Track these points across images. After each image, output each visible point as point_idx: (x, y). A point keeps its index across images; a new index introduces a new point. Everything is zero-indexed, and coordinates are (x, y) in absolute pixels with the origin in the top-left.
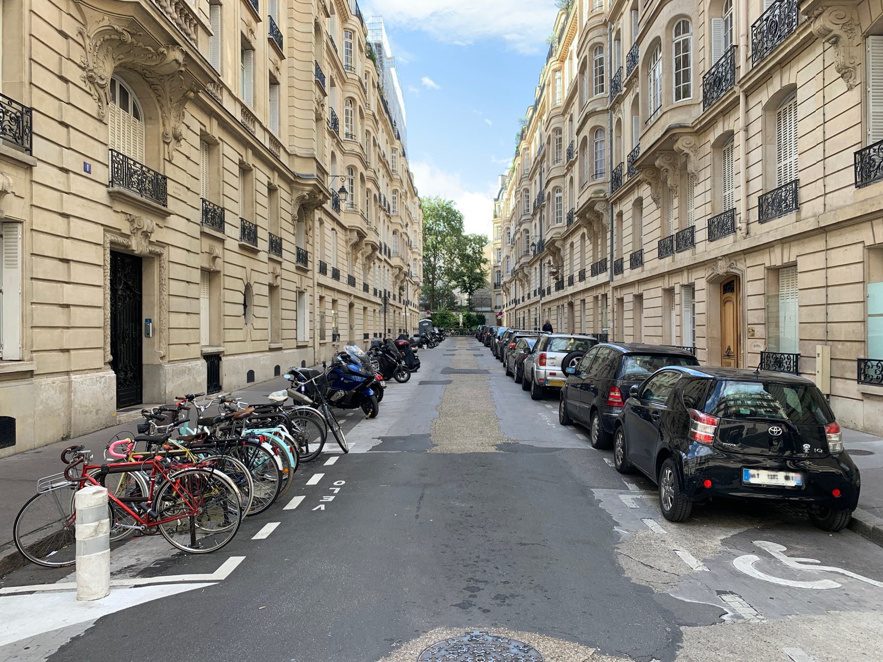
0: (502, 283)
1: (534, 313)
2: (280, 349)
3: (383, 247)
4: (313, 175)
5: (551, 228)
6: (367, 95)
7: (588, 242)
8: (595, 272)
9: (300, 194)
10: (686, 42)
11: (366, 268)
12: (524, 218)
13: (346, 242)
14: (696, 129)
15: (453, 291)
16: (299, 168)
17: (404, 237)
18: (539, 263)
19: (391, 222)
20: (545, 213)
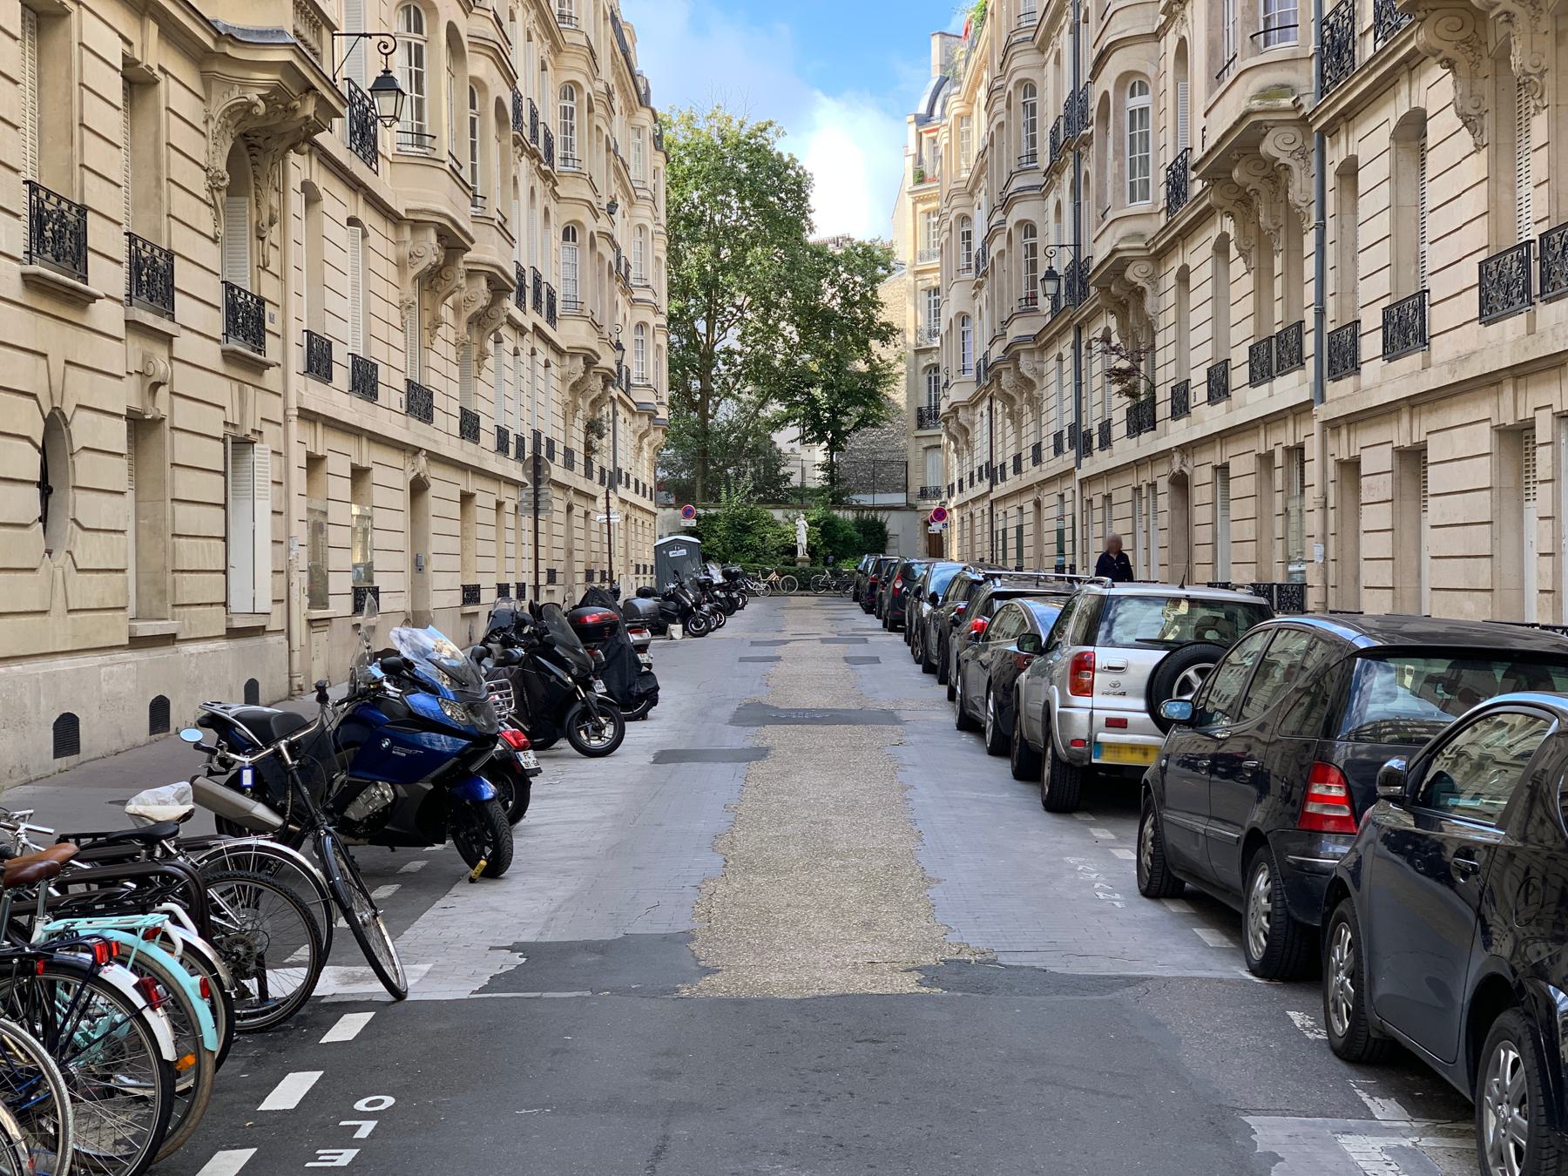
0: (944, 408)
1: (1054, 512)
2: (169, 639)
3: (529, 282)
4: (281, 32)
5: (1110, 216)
7: (1238, 267)
8: (1261, 372)
11: (471, 359)
15: (776, 436)
17: (603, 247)
18: (1070, 338)
19: (557, 198)
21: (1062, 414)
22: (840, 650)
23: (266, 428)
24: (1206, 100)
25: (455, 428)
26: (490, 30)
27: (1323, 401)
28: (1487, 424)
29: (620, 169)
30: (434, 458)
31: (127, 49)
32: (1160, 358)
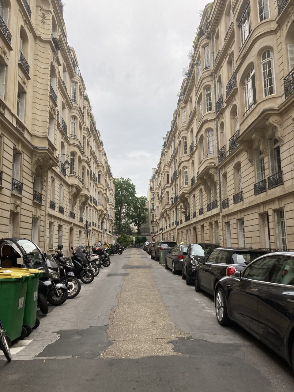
0: (155, 220)
1: (173, 234)
3: (92, 199)
4: (46, 148)
5: (182, 188)
6: (85, 118)
7: (204, 193)
8: (209, 209)
9: (37, 158)
10: (269, 62)
11: (82, 209)
12: (166, 186)
13: (69, 193)
14: (281, 110)
15: (130, 225)
16: (37, 143)
17: (105, 195)
18: (175, 208)
19: (98, 187)
20: (178, 182)
21: (174, 219)
22: (140, 256)
23: (41, 216)
24: (198, 166)
25: (79, 220)
26: (86, 159)
27: (222, 212)
28: (257, 213)
29: (108, 185)
30: (75, 225)
31: (15, 146)
32: (190, 209)
